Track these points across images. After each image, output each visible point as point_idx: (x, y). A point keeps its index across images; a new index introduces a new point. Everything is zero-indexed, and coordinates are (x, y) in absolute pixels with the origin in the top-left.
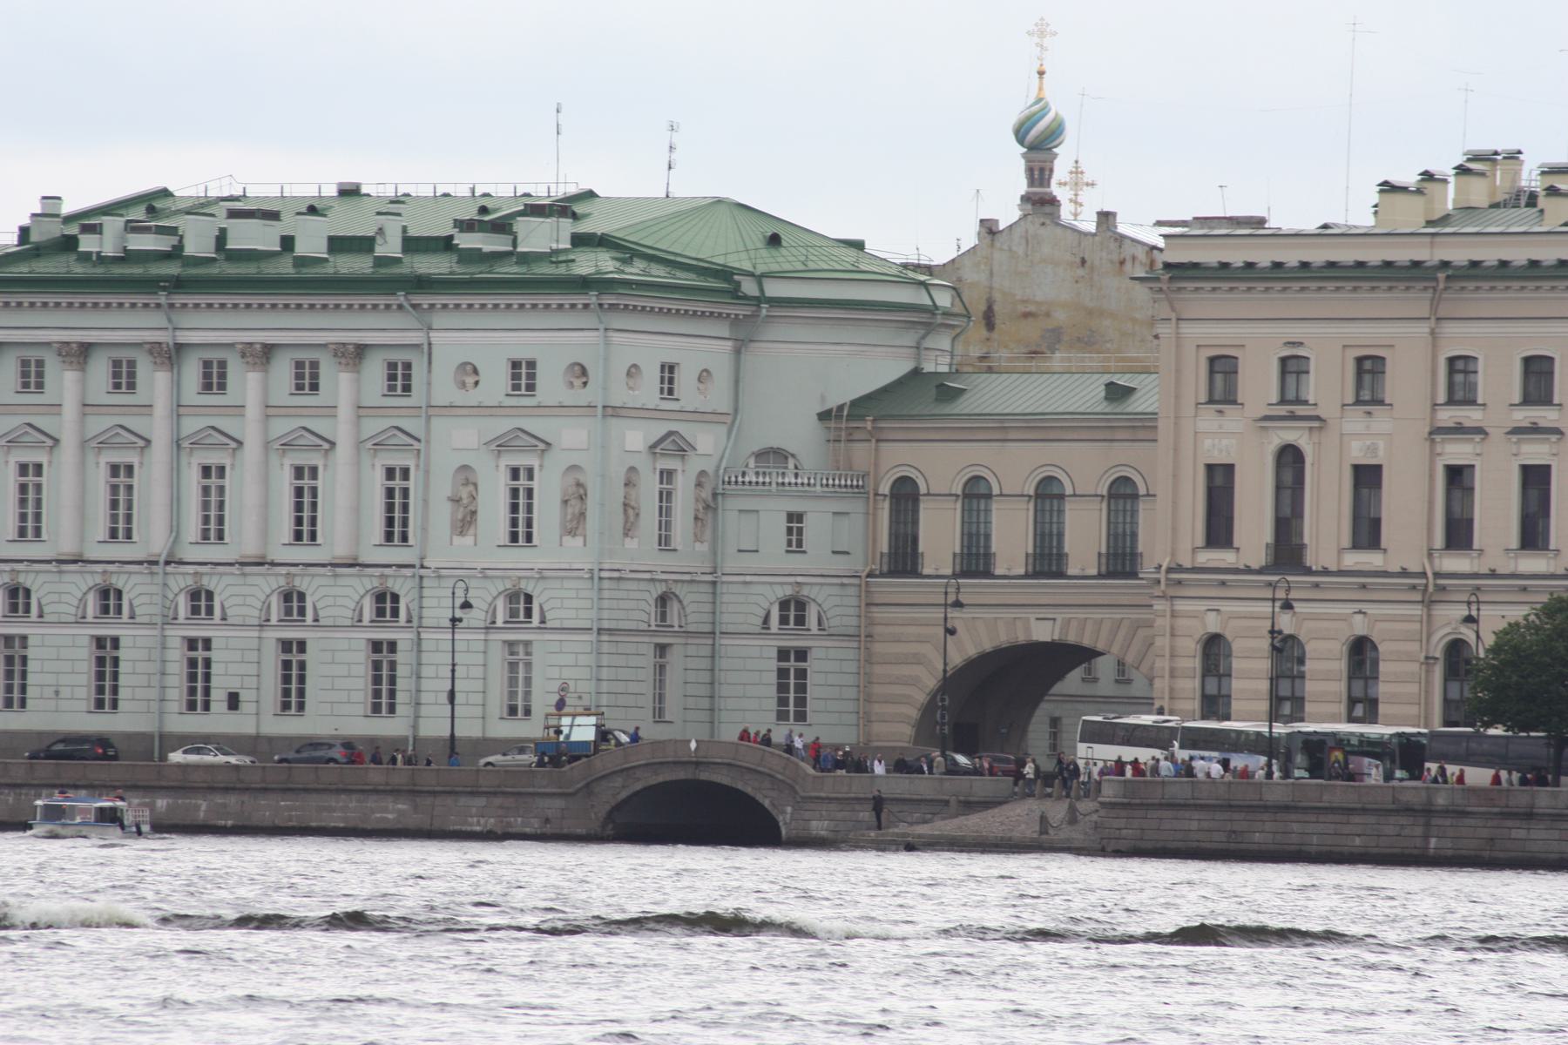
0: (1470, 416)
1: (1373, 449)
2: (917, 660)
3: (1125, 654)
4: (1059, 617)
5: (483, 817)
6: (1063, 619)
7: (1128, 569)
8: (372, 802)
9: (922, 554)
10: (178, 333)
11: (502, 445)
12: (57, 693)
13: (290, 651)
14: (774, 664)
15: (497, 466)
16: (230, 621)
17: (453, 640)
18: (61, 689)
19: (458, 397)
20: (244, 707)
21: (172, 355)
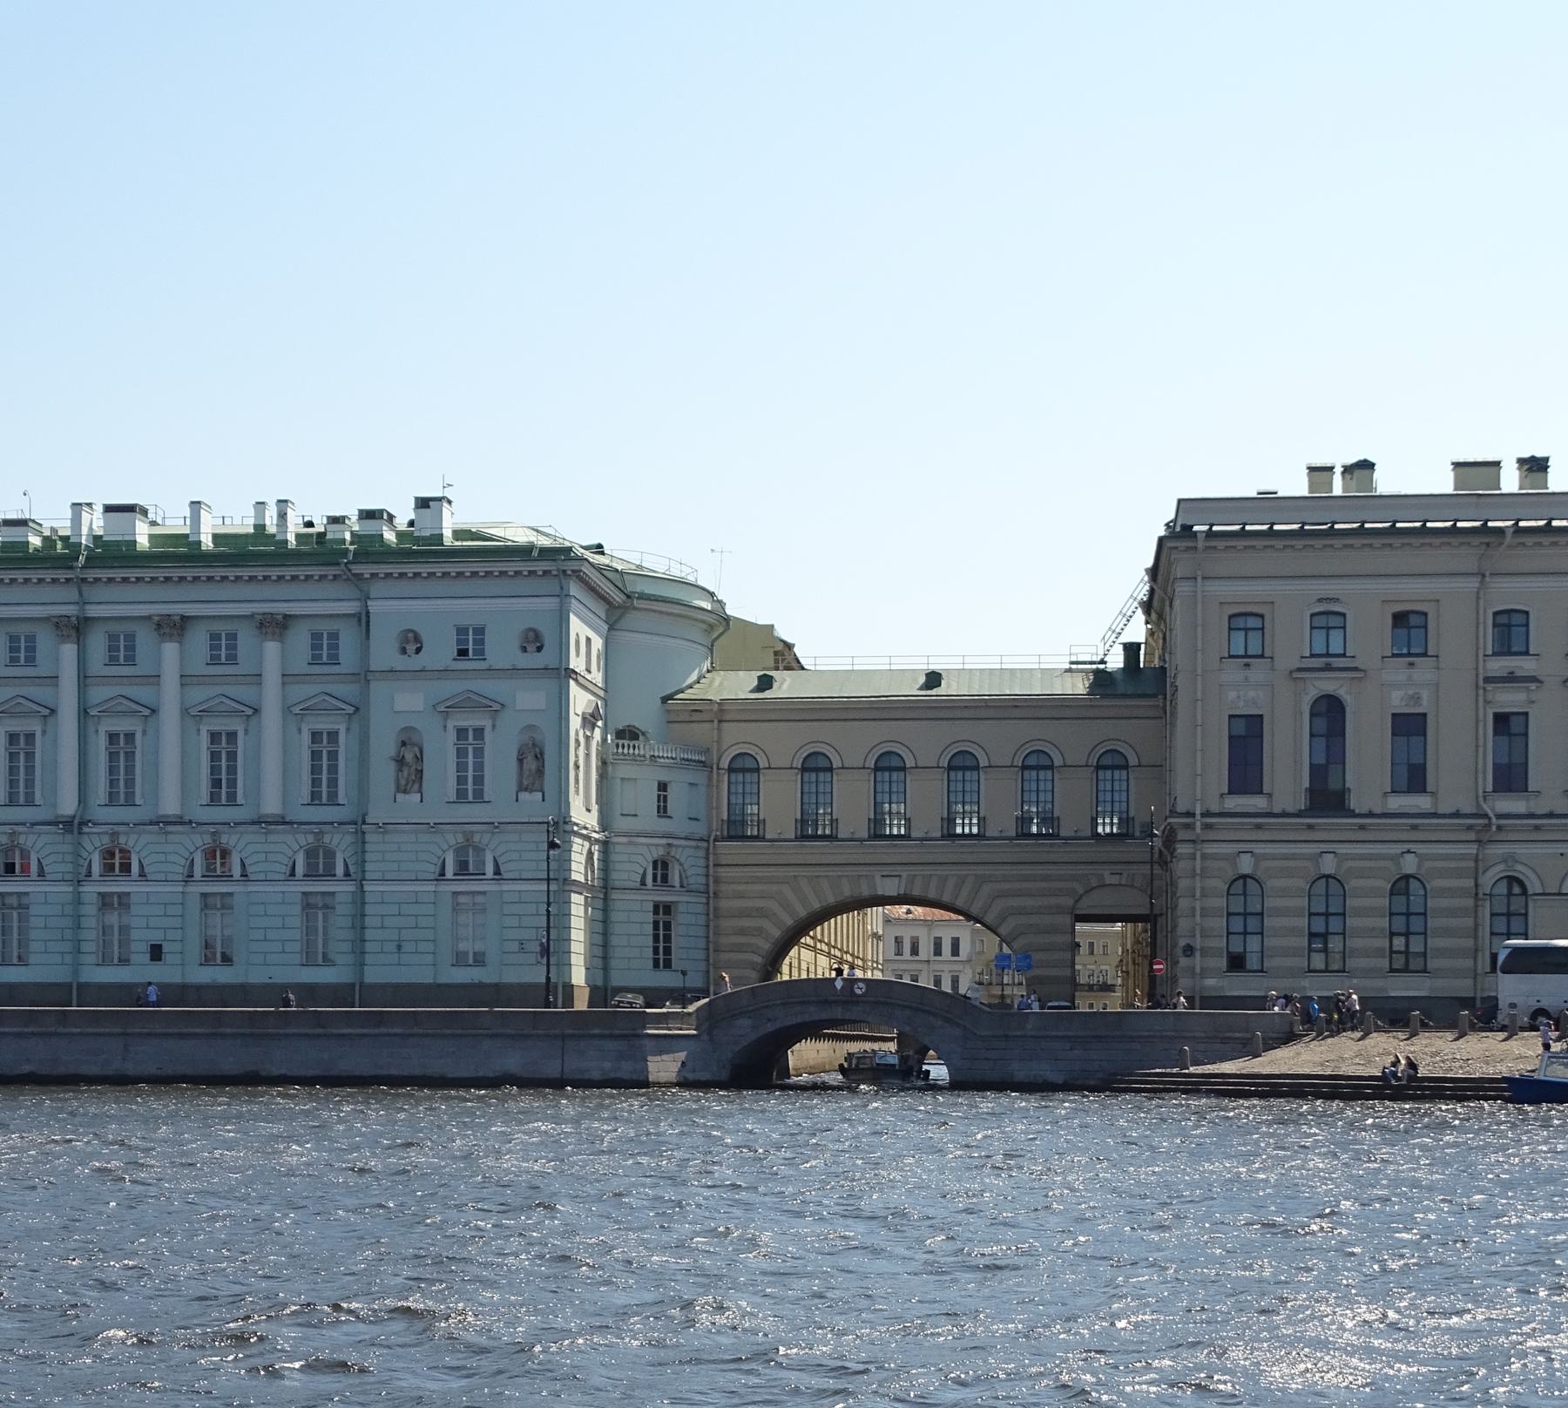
0: (1524, 665)
1: (1416, 699)
2: (762, 913)
3: (986, 912)
6: (908, 875)
10: (87, 607)
11: (448, 709)
12: (399, 947)
14: (650, 917)
15: (445, 727)
16: (48, 877)
18: (403, 944)
19: (400, 662)
20: (167, 958)
21: (77, 628)
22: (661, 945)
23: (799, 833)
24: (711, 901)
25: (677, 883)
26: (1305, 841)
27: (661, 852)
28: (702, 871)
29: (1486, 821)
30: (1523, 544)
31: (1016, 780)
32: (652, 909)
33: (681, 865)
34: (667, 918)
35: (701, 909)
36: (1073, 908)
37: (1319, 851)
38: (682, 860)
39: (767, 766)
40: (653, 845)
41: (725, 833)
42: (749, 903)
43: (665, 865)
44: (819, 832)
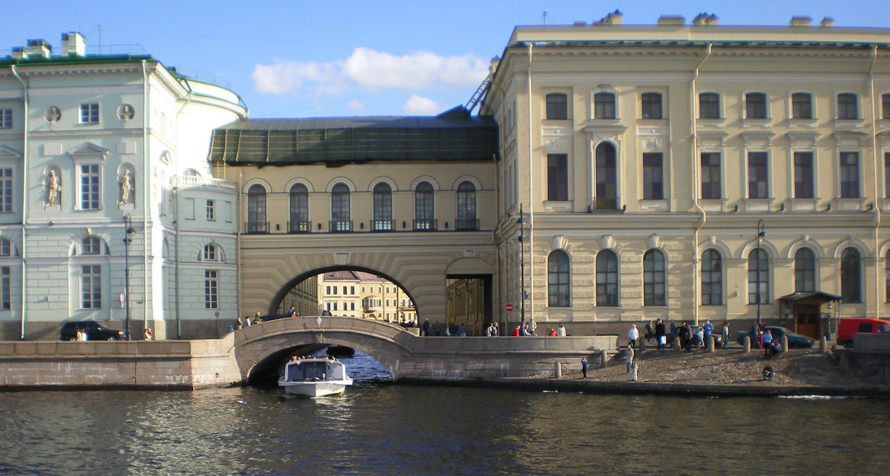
2: (268, 276)
3: (396, 274)
4: (350, 253)
5: (178, 375)
7: (377, 228)
8: (84, 367)
9: (479, 220)
13: (89, 272)
14: (204, 279)
16: (112, 254)
17: (127, 263)
22: (210, 295)
23: (289, 229)
24: (240, 268)
25: (219, 258)
26: (559, 229)
27: (210, 241)
28: (234, 252)
29: (699, 216)
30: (606, 54)
31: (329, 199)
32: (204, 274)
33: (222, 248)
34: (214, 279)
35: (234, 274)
36: (446, 271)
37: (553, 235)
38: (222, 246)
39: (312, 191)
40: (204, 236)
41: (247, 230)
42: (259, 270)
43: (212, 249)
44: (343, 229)
